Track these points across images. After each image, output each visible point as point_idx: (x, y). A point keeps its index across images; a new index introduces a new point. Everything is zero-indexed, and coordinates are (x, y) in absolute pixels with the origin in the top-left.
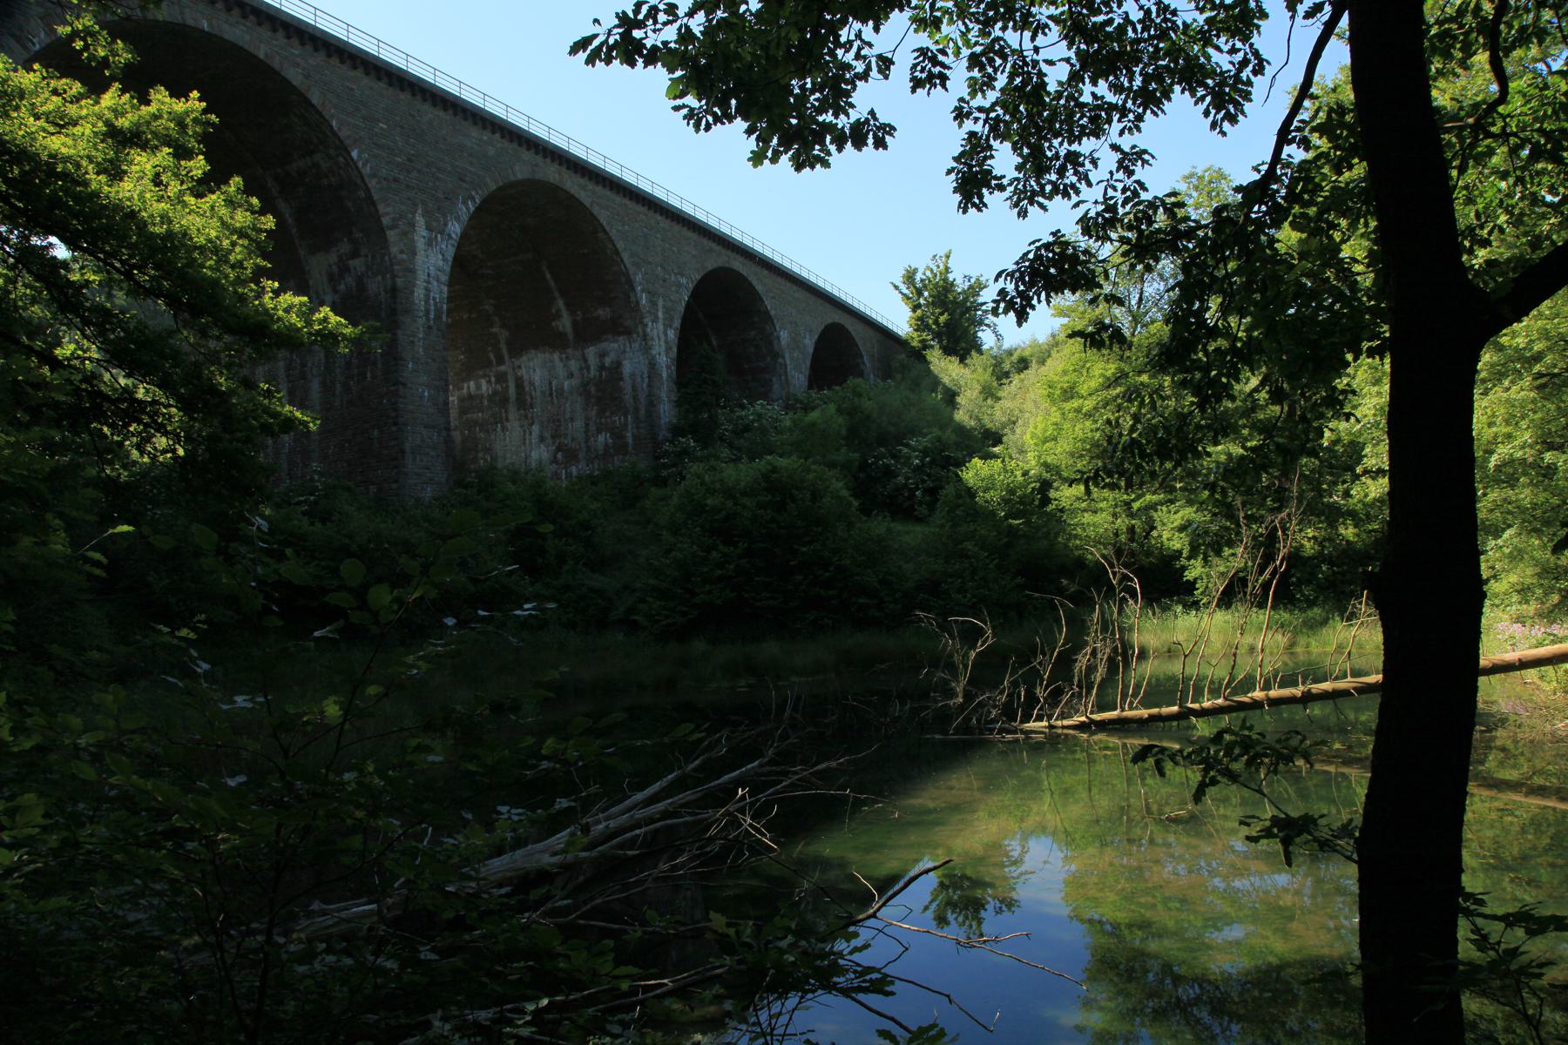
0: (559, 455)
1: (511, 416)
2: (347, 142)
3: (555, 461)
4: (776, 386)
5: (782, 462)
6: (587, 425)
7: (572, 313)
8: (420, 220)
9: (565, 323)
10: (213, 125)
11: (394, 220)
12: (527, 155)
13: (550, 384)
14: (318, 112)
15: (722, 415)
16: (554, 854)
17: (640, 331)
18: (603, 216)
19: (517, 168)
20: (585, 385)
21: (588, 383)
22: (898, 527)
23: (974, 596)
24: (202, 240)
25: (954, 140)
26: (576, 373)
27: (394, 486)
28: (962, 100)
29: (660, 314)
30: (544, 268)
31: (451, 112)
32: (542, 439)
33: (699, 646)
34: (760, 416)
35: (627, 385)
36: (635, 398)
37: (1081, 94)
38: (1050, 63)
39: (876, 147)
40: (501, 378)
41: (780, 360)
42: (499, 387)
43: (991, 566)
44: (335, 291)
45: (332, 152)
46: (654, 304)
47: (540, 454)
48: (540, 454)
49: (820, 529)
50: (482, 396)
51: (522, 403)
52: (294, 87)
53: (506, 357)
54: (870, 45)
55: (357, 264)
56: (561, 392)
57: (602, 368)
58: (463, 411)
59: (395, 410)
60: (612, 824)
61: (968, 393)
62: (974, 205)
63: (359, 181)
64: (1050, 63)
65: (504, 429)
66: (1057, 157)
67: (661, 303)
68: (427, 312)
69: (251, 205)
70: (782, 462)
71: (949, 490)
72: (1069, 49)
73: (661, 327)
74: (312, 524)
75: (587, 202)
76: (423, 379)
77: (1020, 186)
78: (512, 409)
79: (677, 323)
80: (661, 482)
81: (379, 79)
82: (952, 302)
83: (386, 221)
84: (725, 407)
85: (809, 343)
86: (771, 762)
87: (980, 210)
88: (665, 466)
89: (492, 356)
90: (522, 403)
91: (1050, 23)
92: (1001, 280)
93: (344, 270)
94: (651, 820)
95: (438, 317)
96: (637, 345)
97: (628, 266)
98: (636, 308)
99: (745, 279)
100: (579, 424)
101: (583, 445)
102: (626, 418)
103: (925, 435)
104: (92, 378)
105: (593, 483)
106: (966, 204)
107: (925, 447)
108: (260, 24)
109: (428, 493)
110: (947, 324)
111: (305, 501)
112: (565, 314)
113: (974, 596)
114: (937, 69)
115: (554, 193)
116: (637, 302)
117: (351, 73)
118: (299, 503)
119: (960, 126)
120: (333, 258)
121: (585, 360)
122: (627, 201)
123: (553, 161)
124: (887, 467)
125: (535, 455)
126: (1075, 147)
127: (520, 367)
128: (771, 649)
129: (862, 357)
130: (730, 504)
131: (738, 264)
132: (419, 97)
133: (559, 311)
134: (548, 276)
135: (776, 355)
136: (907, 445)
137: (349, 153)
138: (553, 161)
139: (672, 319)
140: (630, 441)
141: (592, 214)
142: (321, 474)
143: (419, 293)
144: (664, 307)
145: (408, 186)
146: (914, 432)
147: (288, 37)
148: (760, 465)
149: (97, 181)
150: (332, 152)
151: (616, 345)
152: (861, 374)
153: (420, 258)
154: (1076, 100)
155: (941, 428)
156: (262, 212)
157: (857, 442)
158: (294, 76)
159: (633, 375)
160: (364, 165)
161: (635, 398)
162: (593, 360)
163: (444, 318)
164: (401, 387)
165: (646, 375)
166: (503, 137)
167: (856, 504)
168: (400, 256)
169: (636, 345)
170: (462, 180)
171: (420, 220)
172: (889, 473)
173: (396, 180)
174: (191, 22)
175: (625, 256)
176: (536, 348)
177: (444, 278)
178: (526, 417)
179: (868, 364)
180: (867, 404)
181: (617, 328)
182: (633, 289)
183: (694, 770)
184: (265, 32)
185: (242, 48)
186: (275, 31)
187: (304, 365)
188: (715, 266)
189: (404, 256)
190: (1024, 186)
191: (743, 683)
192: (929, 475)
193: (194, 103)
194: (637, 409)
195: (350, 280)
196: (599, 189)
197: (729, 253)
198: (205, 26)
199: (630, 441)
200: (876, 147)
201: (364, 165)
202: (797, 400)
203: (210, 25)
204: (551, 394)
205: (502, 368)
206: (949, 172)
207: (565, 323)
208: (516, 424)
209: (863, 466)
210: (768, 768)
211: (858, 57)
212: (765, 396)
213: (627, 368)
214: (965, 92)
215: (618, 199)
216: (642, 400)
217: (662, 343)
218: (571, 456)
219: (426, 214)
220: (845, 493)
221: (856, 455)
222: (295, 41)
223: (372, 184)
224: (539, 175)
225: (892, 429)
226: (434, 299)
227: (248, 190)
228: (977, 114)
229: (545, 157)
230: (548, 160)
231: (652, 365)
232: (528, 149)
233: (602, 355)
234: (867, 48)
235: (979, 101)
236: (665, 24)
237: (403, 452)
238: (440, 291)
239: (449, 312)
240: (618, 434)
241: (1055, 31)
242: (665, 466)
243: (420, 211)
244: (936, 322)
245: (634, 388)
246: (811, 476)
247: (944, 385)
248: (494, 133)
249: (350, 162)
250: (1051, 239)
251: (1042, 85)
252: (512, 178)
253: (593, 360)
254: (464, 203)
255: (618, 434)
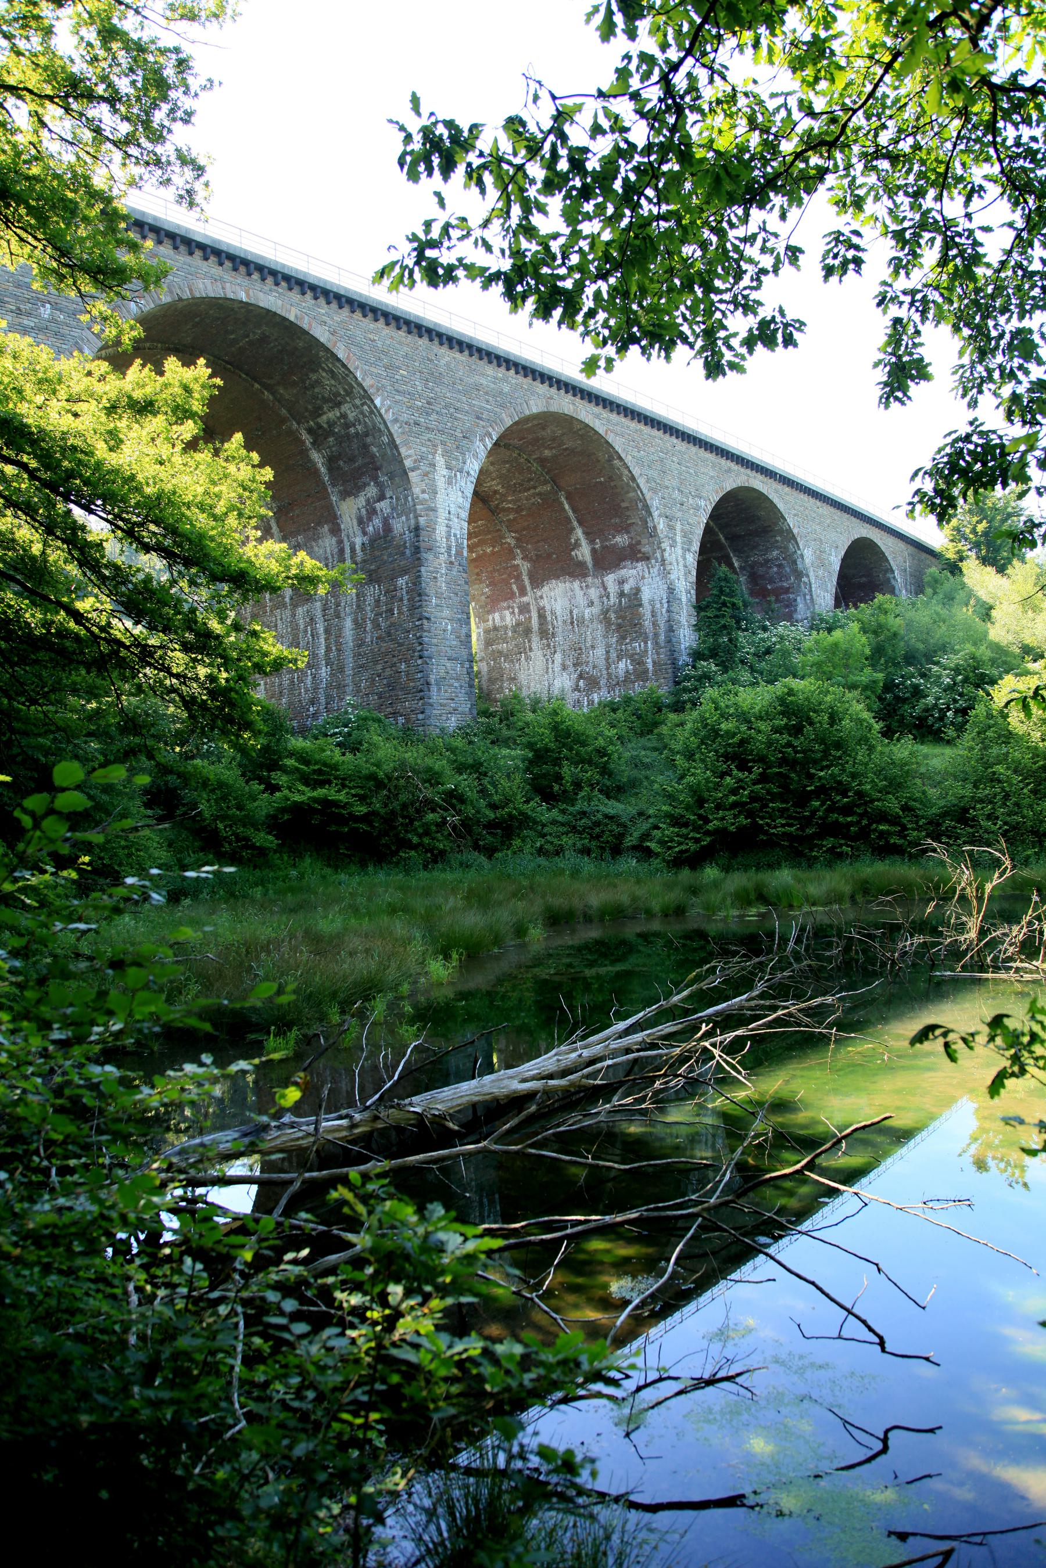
0: (581, 683)
1: (534, 646)
2: (371, 391)
3: (577, 689)
4: (801, 606)
5: (796, 684)
6: (608, 652)
7: (592, 542)
8: (440, 461)
9: (584, 552)
10: (219, 387)
11: (415, 461)
12: (542, 389)
13: (571, 612)
14: (344, 366)
15: (742, 637)
16: (524, 1080)
17: (658, 555)
18: (618, 444)
19: (532, 402)
20: (605, 612)
21: (608, 611)
22: (925, 749)
23: (1005, 823)
24: (188, 498)
25: (879, 326)
26: (596, 601)
27: (421, 716)
28: (884, 283)
29: (678, 539)
30: (563, 499)
31: (466, 353)
32: (564, 668)
33: (711, 872)
34: (782, 638)
35: (646, 611)
36: (655, 624)
37: (1030, 262)
38: (987, 229)
39: (786, 346)
40: (524, 609)
41: (805, 579)
42: (522, 617)
43: (1025, 791)
44: (365, 533)
45: (358, 402)
46: (672, 528)
47: (563, 682)
48: (563, 682)
49: (839, 753)
50: (506, 627)
51: (544, 633)
52: (323, 345)
53: (529, 588)
54: (776, 235)
55: (383, 506)
56: (581, 621)
57: (622, 594)
58: (488, 643)
59: (421, 644)
60: (586, 1053)
61: (1005, 606)
62: (897, 399)
63: (382, 427)
64: (987, 229)
65: (528, 658)
66: (1001, 336)
67: (679, 527)
68: (449, 548)
69: (251, 459)
70: (796, 684)
71: (980, 710)
72: (1013, 211)
73: (680, 552)
74: (344, 754)
75: (601, 431)
76: (446, 613)
77: (968, 374)
78: (535, 638)
79: (696, 546)
80: (678, 707)
81: (399, 328)
82: (991, 509)
83: (408, 463)
84: (746, 630)
85: (835, 562)
86: (762, 996)
87: (903, 403)
88: (686, 690)
89: (514, 587)
90: (544, 633)
91: (985, 184)
92: (919, 479)
93: (372, 512)
94: (628, 1051)
95: (459, 553)
96: (656, 570)
97: (645, 491)
98: (653, 534)
99: (766, 499)
100: (600, 651)
101: (605, 672)
102: (646, 643)
103: (956, 653)
104: (106, 628)
105: (614, 710)
106: (887, 399)
107: (957, 665)
108: (290, 289)
109: (453, 723)
110: (986, 534)
111: (340, 733)
112: (584, 542)
113: (1005, 823)
114: (850, 254)
115: (568, 422)
116: (655, 527)
117: (373, 326)
118: (335, 734)
119: (885, 312)
120: (361, 501)
121: (605, 589)
122: (641, 426)
123: (567, 392)
124: (916, 687)
125: (557, 684)
126: (1026, 323)
127: (541, 597)
128: (784, 877)
129: (893, 572)
130: (744, 728)
131: (758, 483)
132: (436, 342)
133: (577, 540)
134: (567, 507)
135: (799, 575)
136: (937, 663)
137: (372, 401)
138: (567, 392)
139: (690, 542)
140: (650, 666)
141: (607, 442)
142: (353, 706)
143: (441, 530)
144: (682, 530)
145: (427, 428)
146: (944, 648)
147: (316, 298)
148: (779, 688)
149: (101, 450)
150: (358, 402)
151: (634, 572)
152: (892, 592)
153: (441, 497)
154: (1025, 270)
155: (975, 644)
156: (261, 466)
157: (882, 661)
158: (321, 334)
159: (652, 602)
160: (387, 411)
161: (655, 624)
162: (612, 588)
163: (465, 554)
164: (425, 622)
165: (665, 601)
166: (517, 373)
167: (877, 727)
168: (422, 496)
169: (655, 571)
170: (478, 418)
171: (440, 461)
172: (917, 693)
173: (417, 424)
174: (231, 296)
175: (641, 481)
176: (557, 577)
177: (465, 515)
178: (548, 645)
179: (899, 579)
180: (895, 623)
181: (634, 554)
182: (650, 514)
183: (683, 1000)
184: (295, 296)
185: (268, 311)
186: (303, 293)
187: (338, 605)
188: (735, 486)
189: (426, 496)
190: (972, 374)
191: (753, 911)
192: (961, 695)
193: (201, 369)
194: (656, 635)
195: (377, 522)
196: (614, 417)
197: (748, 471)
198: (243, 297)
199: (650, 666)
200: (786, 346)
201: (387, 411)
202: (822, 620)
203: (248, 295)
204: (572, 623)
205: (525, 599)
206: (876, 365)
207: (584, 552)
208: (540, 653)
209: (890, 686)
210: (753, 1003)
211: (763, 250)
212: (790, 617)
213: (646, 595)
214: (886, 273)
215: (634, 425)
216: (662, 626)
217: (681, 567)
218: (593, 683)
219: (446, 453)
220: (866, 715)
221: (880, 676)
222: (322, 301)
223: (395, 429)
224: (554, 408)
225: (921, 646)
226: (455, 535)
227: (249, 446)
228: (902, 298)
229: (559, 389)
230: (562, 392)
231: (671, 590)
232: (542, 383)
233: (621, 582)
234: (773, 239)
235: (902, 283)
236: (460, 239)
237: (428, 684)
238: (461, 527)
239: (471, 548)
240: (638, 661)
241: (993, 190)
242: (686, 690)
243: (439, 452)
244: (974, 531)
245: (653, 614)
246: (829, 698)
247: (978, 599)
248: (508, 369)
249: (375, 411)
250: (969, 429)
251: (976, 259)
252: (527, 413)
253: (612, 588)
254: (482, 440)
255: (638, 661)
